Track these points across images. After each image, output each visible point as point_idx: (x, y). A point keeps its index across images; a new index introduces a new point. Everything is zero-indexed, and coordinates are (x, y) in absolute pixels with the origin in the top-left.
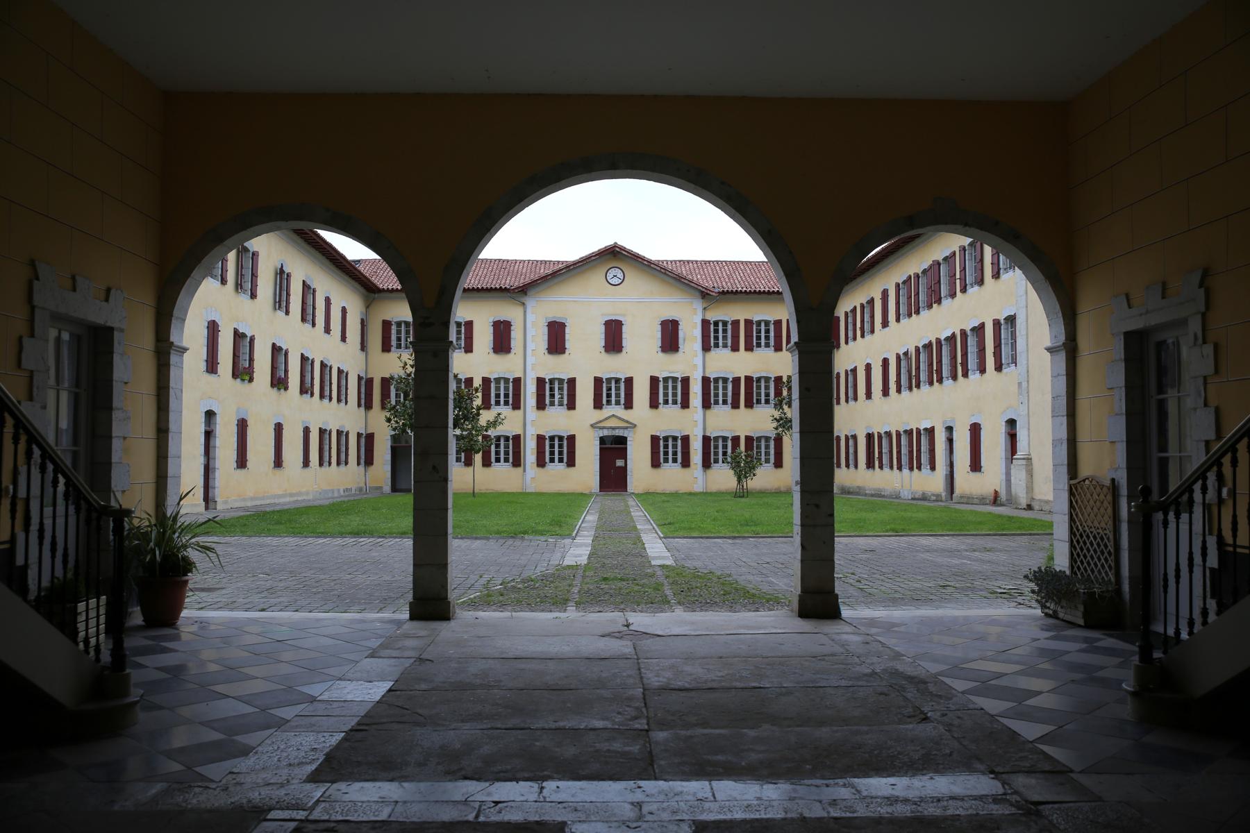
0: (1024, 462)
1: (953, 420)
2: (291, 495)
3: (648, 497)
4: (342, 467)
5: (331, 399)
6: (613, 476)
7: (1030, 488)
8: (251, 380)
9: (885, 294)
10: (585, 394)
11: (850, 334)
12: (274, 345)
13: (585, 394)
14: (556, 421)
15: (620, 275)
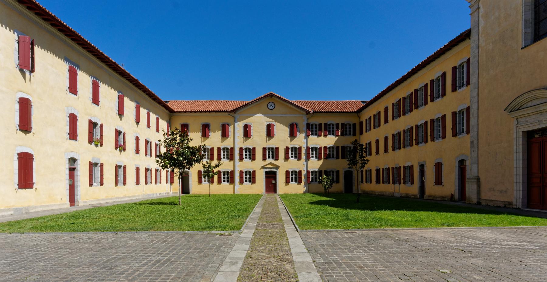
0: (476, 181)
1: (425, 162)
2: (129, 197)
3: (284, 197)
4: (158, 184)
5: (151, 156)
6: (271, 187)
7: (479, 193)
8: (101, 145)
9: (386, 109)
10: (259, 154)
11: (368, 128)
12: (116, 130)
13: (259, 154)
14: (247, 165)
15: (273, 105)
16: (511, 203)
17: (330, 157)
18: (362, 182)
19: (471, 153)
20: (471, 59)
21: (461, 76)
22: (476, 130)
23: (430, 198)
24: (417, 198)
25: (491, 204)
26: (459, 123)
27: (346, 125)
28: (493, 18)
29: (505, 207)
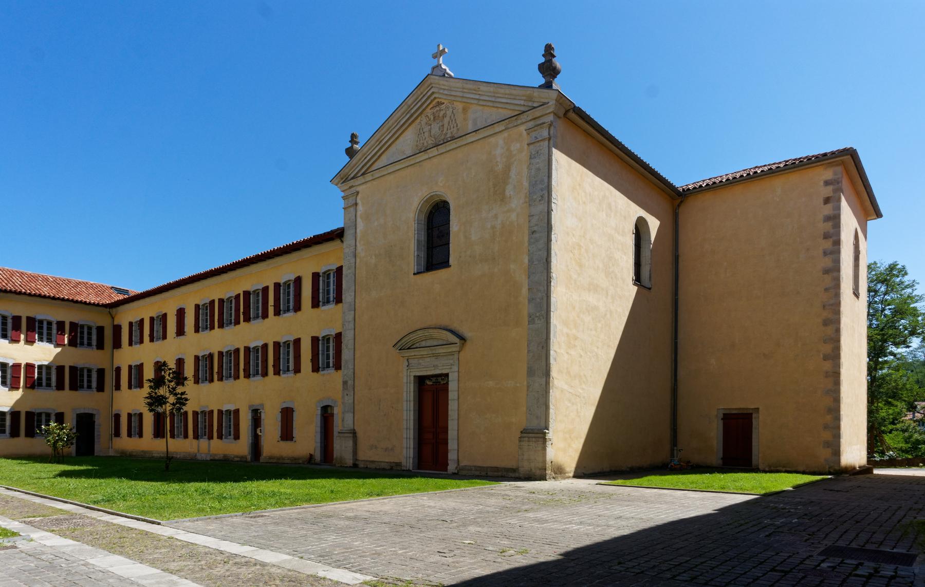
7: (355, 452)
16: (399, 464)
17: (40, 385)
18: (117, 434)
19: (343, 397)
20: (344, 269)
21: (329, 288)
22: (351, 367)
23: (271, 461)
24: (246, 462)
25: (373, 466)
26: (323, 354)
27: (82, 327)
28: (376, 224)
29: (391, 469)
